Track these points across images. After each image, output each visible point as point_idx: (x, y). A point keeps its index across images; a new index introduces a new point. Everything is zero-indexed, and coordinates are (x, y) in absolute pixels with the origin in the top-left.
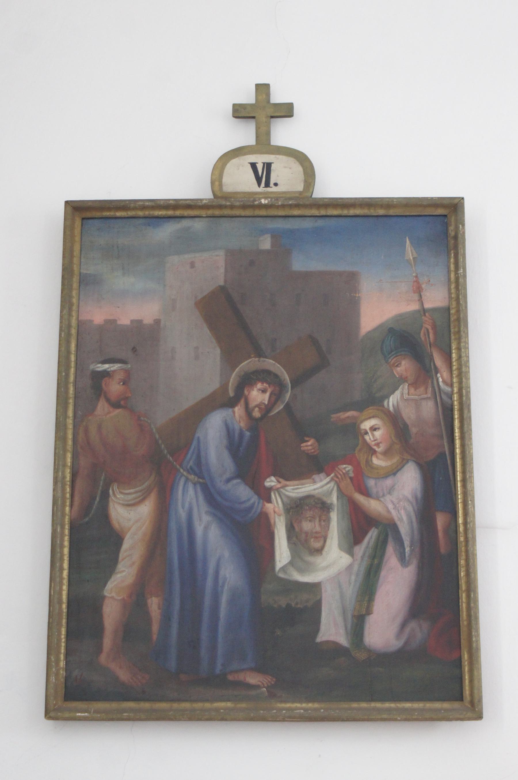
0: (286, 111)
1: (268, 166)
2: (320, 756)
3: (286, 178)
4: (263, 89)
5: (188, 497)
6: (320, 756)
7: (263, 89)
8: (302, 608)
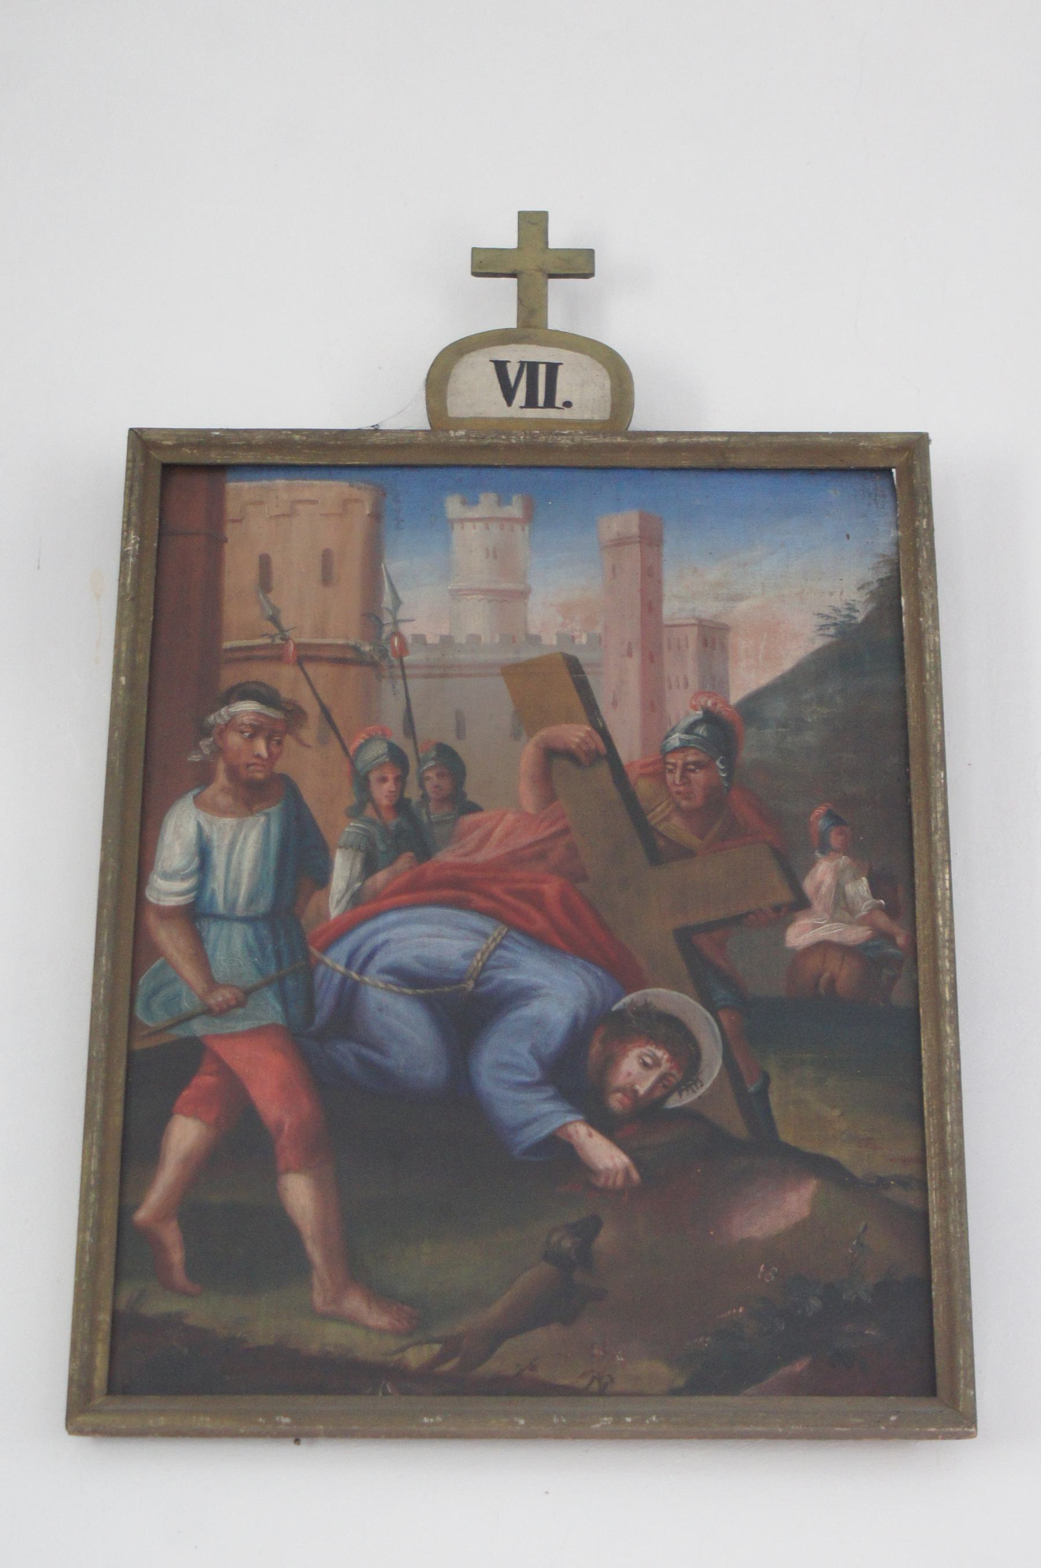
1: (552, 369)
2: (848, 537)
3: (582, 392)
4: (533, 224)
6: (848, 537)
7: (533, 224)
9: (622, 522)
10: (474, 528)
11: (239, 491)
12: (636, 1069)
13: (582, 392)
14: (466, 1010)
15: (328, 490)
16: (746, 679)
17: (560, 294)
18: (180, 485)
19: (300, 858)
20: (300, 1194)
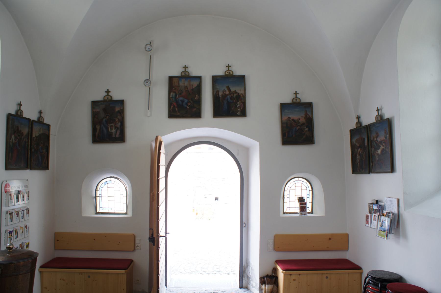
0: (298, 94)
3: (298, 100)
5: (102, 126)
7: (296, 92)
8: (111, 134)
9: (189, 80)
10: (183, 80)
11: (173, 79)
12: (189, 104)
13: (187, 74)
14: (183, 101)
15: (177, 79)
16: (194, 87)
17: (230, 68)
18: (171, 79)
19: (176, 95)
20: (176, 109)
